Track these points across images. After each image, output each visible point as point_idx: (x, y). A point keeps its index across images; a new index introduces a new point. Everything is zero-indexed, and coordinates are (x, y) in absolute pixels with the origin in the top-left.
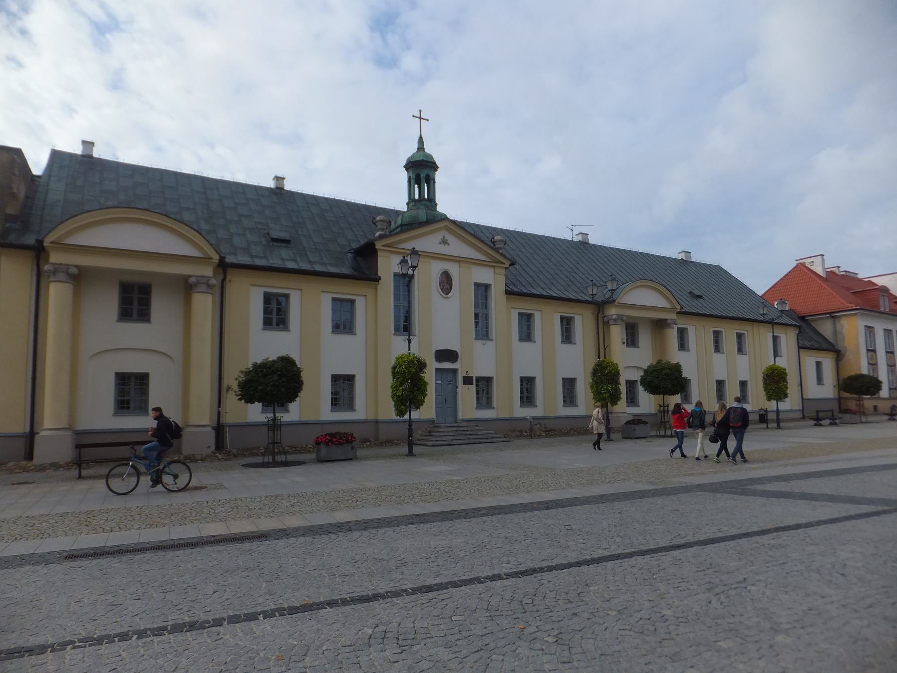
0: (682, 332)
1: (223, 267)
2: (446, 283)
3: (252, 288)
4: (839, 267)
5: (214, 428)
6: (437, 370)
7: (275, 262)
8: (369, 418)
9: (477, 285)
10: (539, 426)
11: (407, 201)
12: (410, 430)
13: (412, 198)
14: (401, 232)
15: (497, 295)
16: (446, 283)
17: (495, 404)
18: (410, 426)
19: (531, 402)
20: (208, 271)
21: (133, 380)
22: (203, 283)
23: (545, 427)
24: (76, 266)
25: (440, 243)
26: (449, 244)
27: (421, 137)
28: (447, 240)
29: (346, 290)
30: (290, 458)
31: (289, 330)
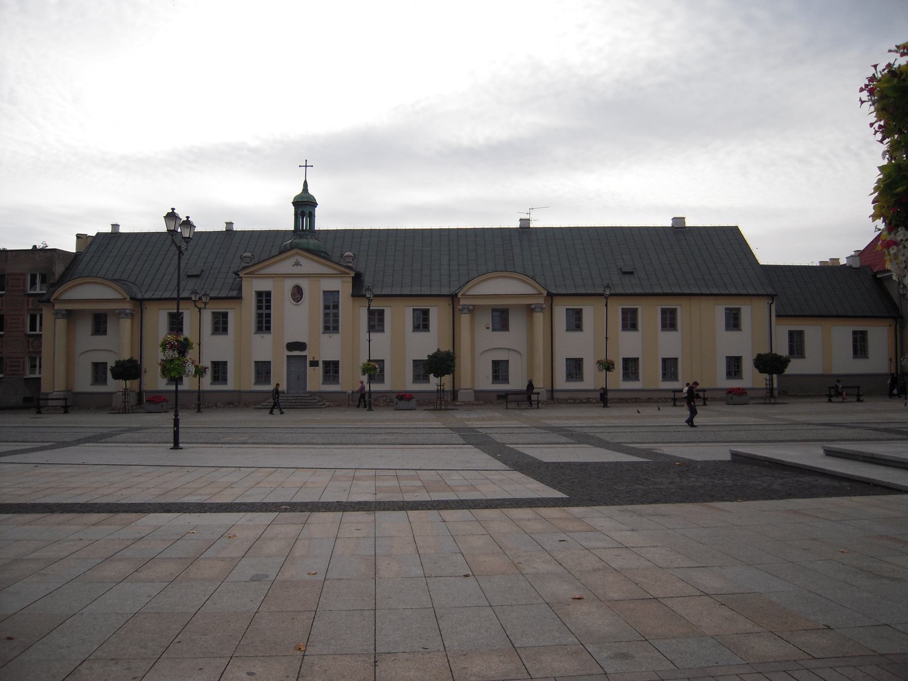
1: (551, 296)
2: (297, 294)
6: (288, 356)
8: (236, 389)
16: (297, 294)
18: (199, 395)
20: (541, 301)
25: (293, 265)
26: (301, 265)
28: (299, 262)
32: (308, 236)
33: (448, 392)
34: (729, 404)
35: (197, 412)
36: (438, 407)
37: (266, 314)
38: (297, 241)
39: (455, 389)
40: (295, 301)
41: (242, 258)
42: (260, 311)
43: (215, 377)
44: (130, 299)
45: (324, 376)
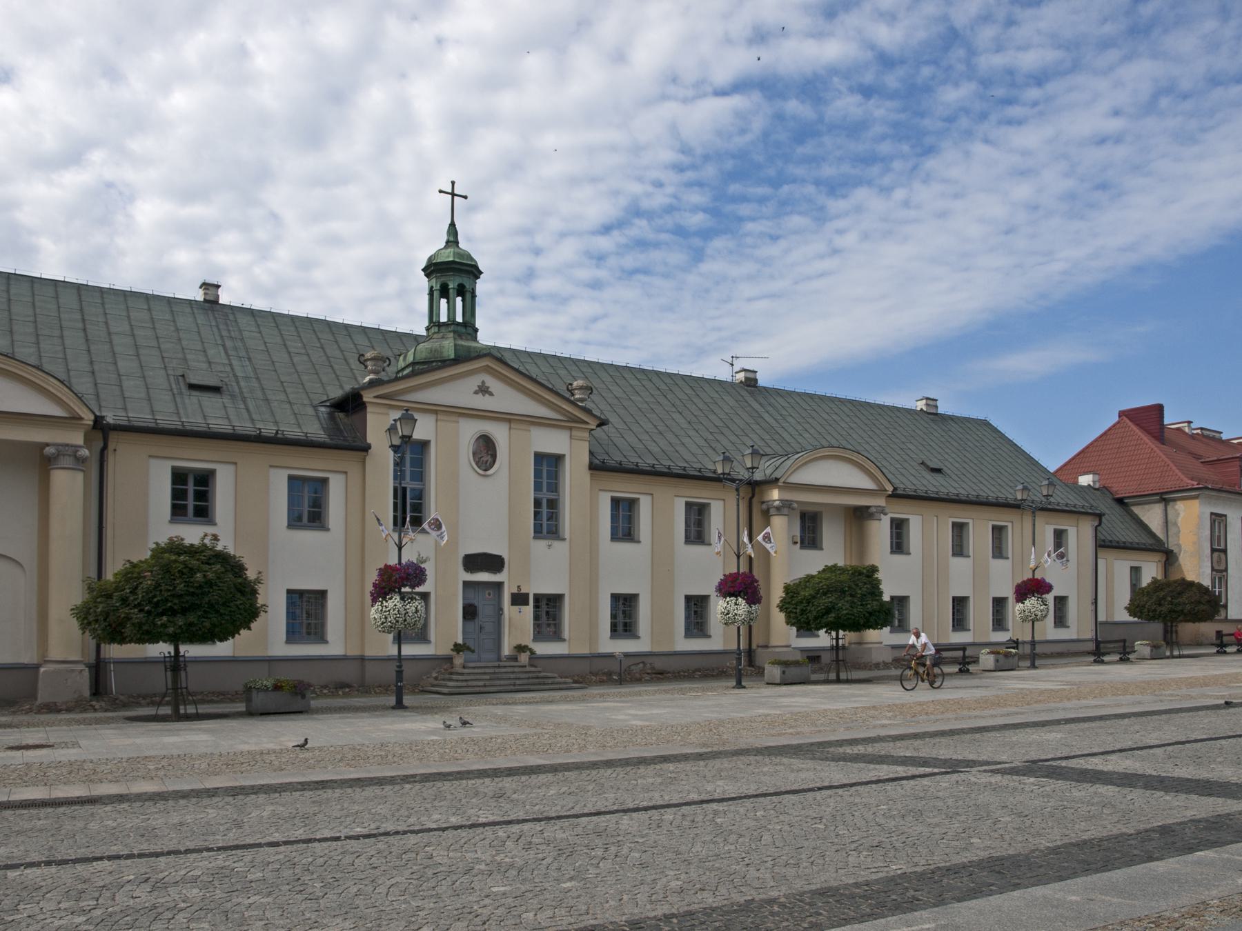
0: (899, 527)
2: (486, 451)
4: (1190, 422)
5: (89, 666)
6: (467, 584)
7: (194, 420)
9: (540, 457)
10: (641, 665)
11: (427, 324)
12: (399, 673)
13: (434, 320)
14: (413, 374)
15: (575, 475)
16: (486, 451)
17: (566, 634)
19: (630, 631)
20: (77, 438)
22: (70, 455)
23: (653, 668)
25: (476, 393)
26: (491, 394)
27: (452, 225)
28: (488, 388)
29: (310, 466)
30: (203, 709)
36: (833, 676)
37: (548, 500)
40: (479, 467)
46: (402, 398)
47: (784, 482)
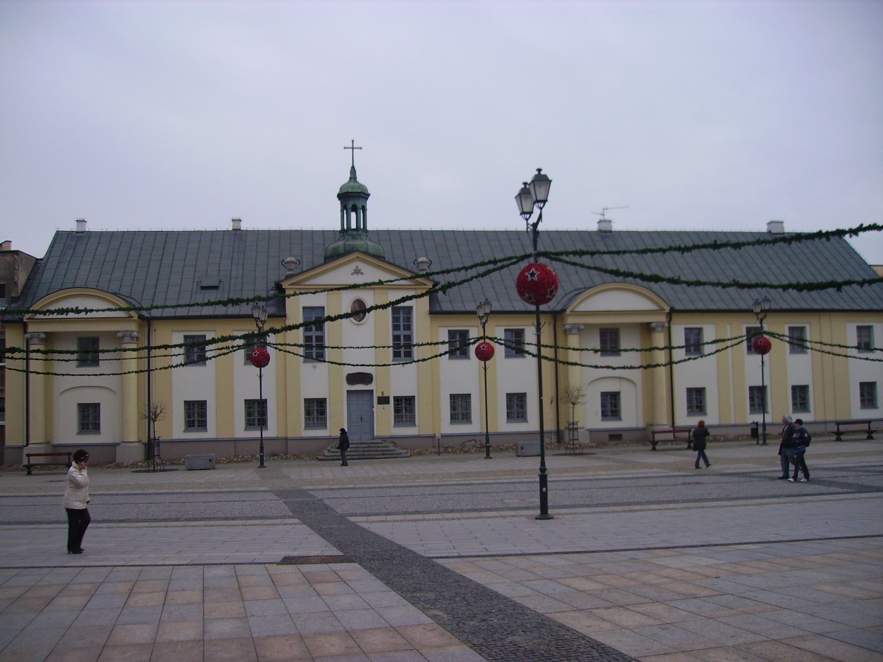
3: (174, 334)
10: (473, 442)
18: (262, 444)
21: (196, 406)
24: (44, 333)
25: (353, 274)
26: (362, 273)
27: (353, 168)
28: (360, 270)
31: (470, 359)
32: (362, 237)
33: (550, 432)
34: (519, 456)
35: (485, 458)
37: (405, 336)
38: (351, 242)
39: (560, 429)
41: (283, 263)
42: (397, 333)
43: (83, 424)
44: (138, 318)
45: (306, 419)
46: (303, 284)
47: (571, 311)
